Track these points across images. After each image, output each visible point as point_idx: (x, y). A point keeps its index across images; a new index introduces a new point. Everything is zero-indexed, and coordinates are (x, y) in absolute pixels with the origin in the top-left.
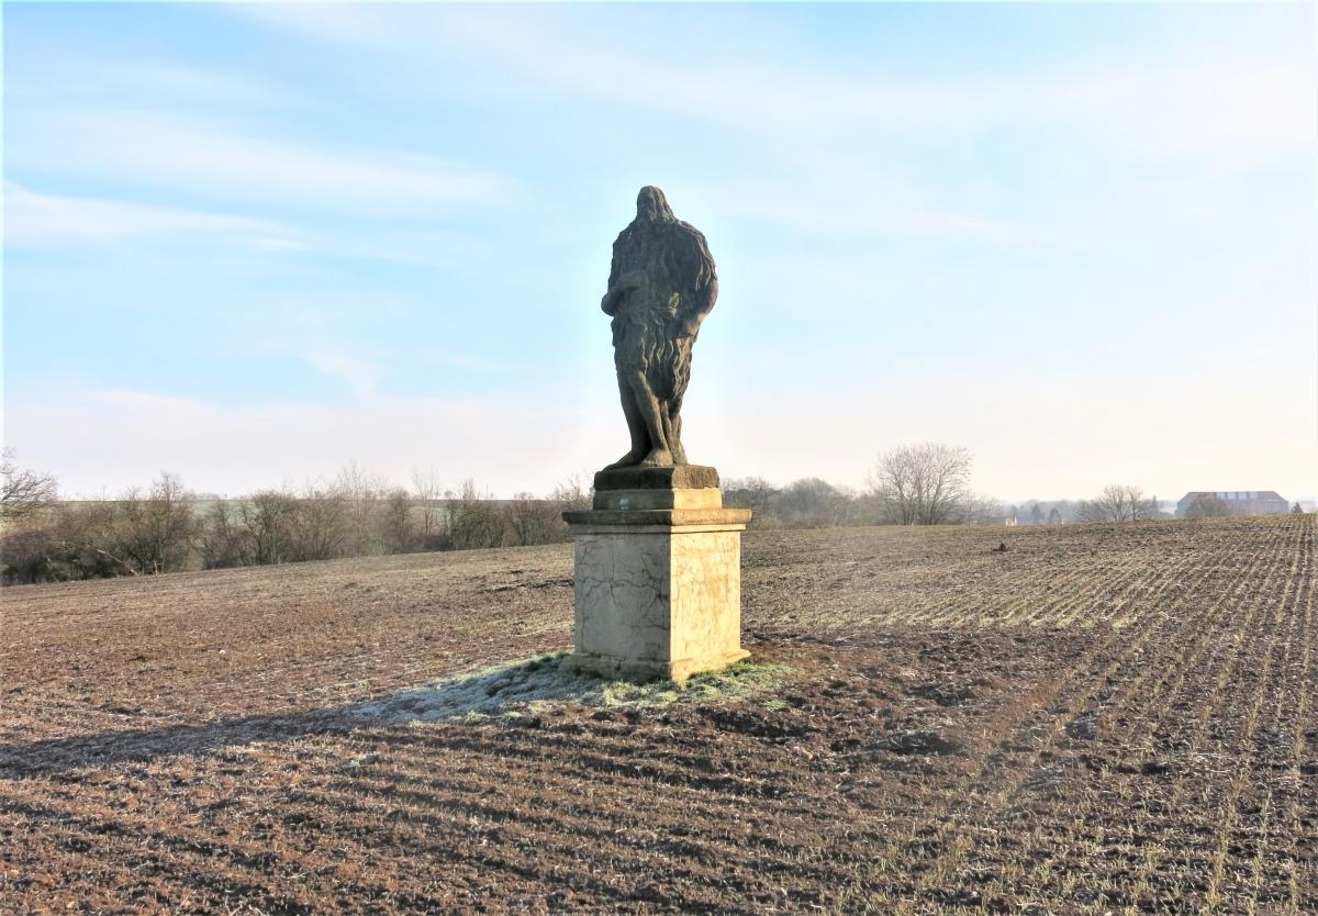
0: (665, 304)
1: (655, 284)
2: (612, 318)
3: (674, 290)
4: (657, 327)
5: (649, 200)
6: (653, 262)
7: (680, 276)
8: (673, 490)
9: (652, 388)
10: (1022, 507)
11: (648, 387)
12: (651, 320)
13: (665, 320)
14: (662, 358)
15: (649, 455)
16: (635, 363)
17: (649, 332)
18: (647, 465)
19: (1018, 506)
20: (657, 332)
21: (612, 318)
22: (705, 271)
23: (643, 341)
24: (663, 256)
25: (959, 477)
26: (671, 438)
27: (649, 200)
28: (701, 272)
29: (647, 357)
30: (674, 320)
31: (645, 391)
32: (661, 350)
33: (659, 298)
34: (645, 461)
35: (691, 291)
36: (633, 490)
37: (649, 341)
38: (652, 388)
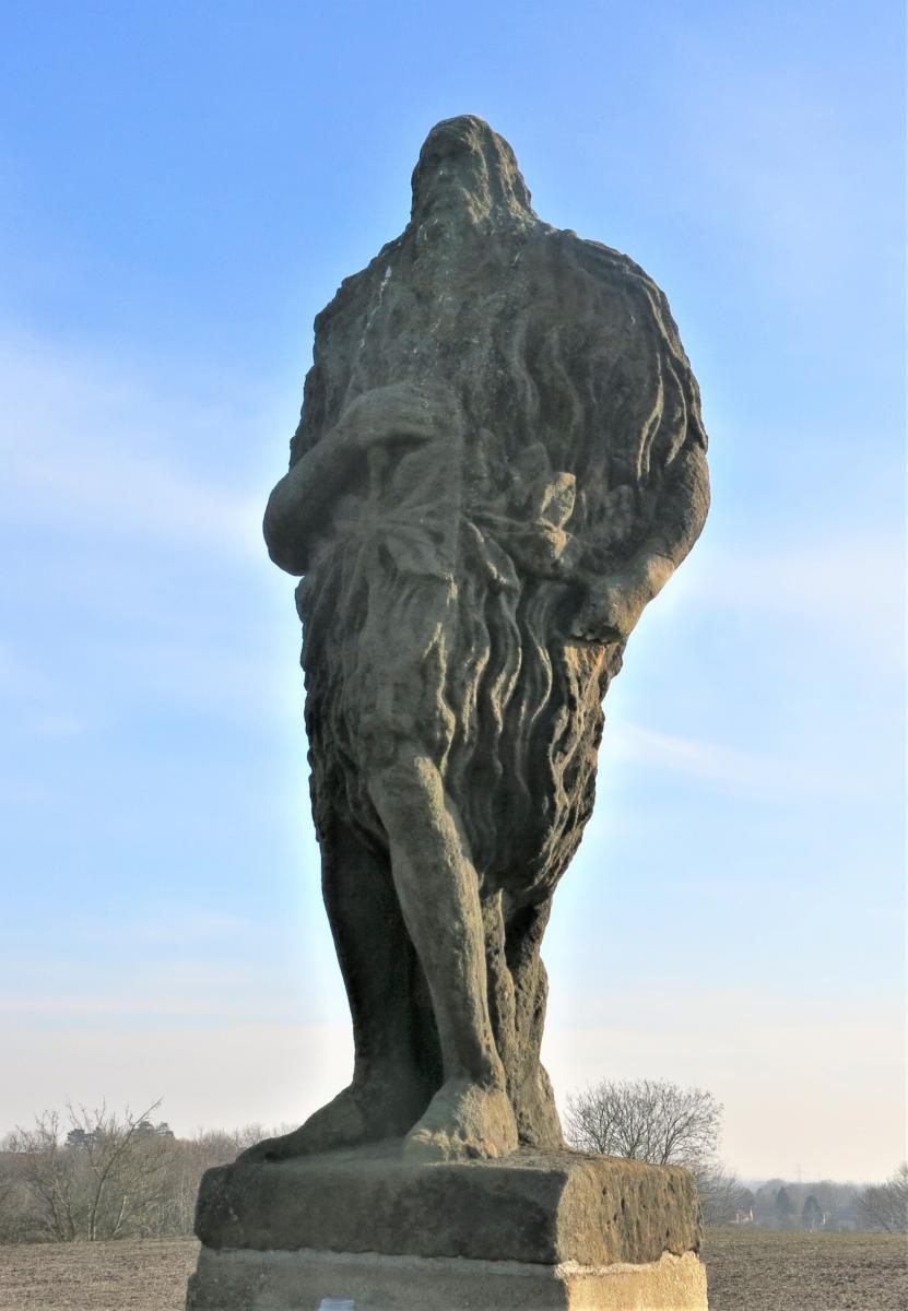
0: (523, 510)
1: (486, 433)
2: (296, 581)
3: (558, 464)
4: (494, 589)
5: (454, 156)
6: (481, 352)
7: (578, 410)
8: (566, 1268)
9: (438, 835)
10: (760, 1190)
11: (446, 822)
12: (472, 563)
13: (523, 571)
14: (511, 709)
15: (437, 1105)
16: (406, 722)
17: (462, 604)
18: (437, 1152)
19: (754, 1190)
20: (492, 604)
21: (296, 581)
22: (669, 409)
23: (441, 638)
24: (518, 338)
25: (699, 1143)
26: (512, 1040)
27: (454, 156)
28: (658, 410)
29: (456, 706)
30: (556, 577)
31: (437, 840)
32: (507, 682)
33: (504, 484)
34: (422, 1134)
35: (618, 476)
36: (371, 1259)
37: (464, 641)
38: (438, 835)
